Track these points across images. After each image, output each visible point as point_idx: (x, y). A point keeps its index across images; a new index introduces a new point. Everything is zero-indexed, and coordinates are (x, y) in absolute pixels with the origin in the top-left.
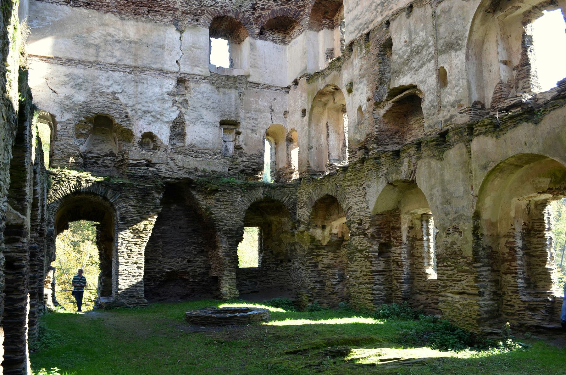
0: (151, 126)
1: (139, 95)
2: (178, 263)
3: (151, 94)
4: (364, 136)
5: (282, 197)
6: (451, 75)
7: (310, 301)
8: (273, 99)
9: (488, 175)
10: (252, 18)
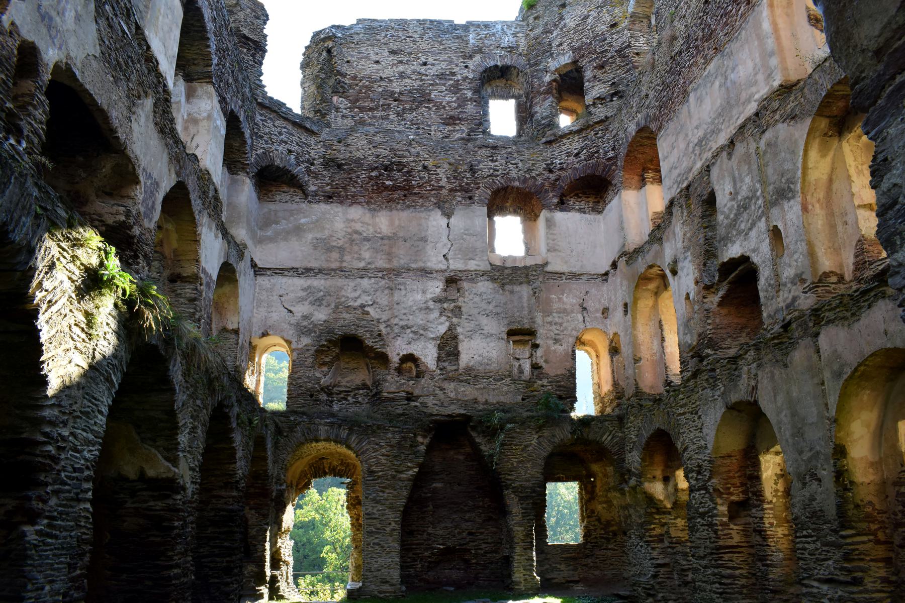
0: (411, 346)
1: (395, 306)
2: (454, 536)
3: (410, 303)
4: (695, 338)
5: (602, 437)
6: (787, 237)
7: (649, 595)
8: (584, 292)
9: (845, 387)
10: (546, 184)
